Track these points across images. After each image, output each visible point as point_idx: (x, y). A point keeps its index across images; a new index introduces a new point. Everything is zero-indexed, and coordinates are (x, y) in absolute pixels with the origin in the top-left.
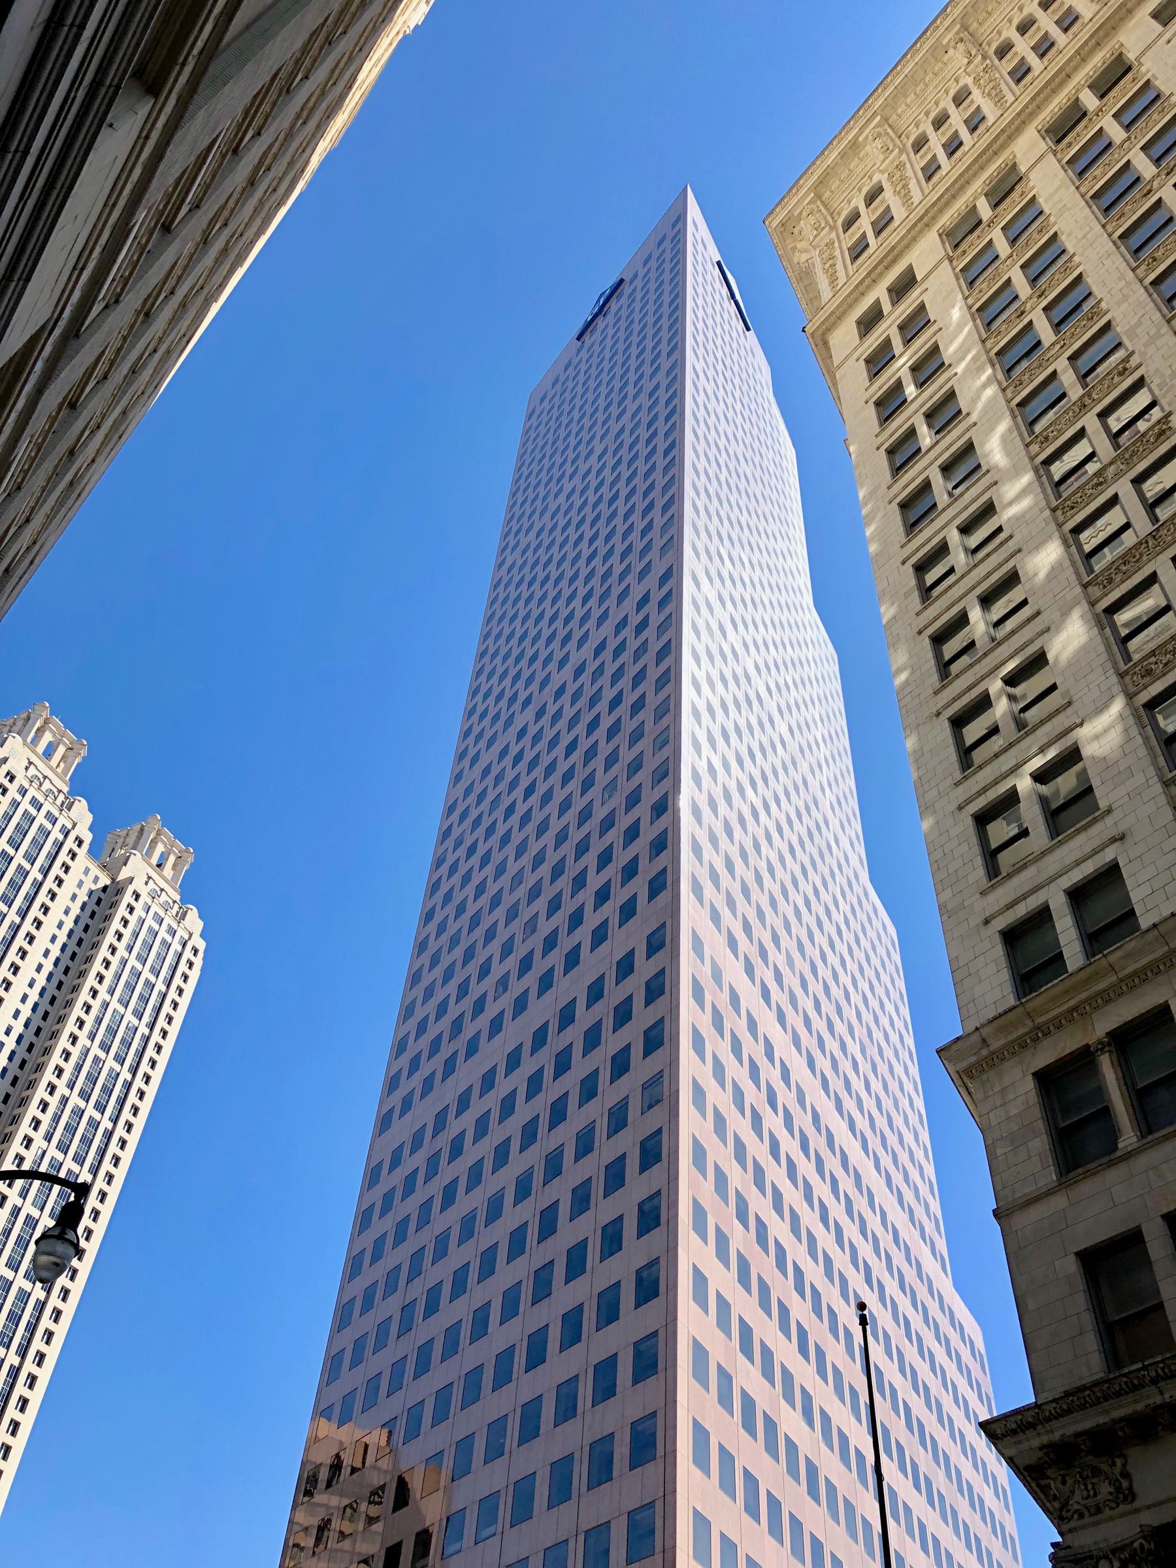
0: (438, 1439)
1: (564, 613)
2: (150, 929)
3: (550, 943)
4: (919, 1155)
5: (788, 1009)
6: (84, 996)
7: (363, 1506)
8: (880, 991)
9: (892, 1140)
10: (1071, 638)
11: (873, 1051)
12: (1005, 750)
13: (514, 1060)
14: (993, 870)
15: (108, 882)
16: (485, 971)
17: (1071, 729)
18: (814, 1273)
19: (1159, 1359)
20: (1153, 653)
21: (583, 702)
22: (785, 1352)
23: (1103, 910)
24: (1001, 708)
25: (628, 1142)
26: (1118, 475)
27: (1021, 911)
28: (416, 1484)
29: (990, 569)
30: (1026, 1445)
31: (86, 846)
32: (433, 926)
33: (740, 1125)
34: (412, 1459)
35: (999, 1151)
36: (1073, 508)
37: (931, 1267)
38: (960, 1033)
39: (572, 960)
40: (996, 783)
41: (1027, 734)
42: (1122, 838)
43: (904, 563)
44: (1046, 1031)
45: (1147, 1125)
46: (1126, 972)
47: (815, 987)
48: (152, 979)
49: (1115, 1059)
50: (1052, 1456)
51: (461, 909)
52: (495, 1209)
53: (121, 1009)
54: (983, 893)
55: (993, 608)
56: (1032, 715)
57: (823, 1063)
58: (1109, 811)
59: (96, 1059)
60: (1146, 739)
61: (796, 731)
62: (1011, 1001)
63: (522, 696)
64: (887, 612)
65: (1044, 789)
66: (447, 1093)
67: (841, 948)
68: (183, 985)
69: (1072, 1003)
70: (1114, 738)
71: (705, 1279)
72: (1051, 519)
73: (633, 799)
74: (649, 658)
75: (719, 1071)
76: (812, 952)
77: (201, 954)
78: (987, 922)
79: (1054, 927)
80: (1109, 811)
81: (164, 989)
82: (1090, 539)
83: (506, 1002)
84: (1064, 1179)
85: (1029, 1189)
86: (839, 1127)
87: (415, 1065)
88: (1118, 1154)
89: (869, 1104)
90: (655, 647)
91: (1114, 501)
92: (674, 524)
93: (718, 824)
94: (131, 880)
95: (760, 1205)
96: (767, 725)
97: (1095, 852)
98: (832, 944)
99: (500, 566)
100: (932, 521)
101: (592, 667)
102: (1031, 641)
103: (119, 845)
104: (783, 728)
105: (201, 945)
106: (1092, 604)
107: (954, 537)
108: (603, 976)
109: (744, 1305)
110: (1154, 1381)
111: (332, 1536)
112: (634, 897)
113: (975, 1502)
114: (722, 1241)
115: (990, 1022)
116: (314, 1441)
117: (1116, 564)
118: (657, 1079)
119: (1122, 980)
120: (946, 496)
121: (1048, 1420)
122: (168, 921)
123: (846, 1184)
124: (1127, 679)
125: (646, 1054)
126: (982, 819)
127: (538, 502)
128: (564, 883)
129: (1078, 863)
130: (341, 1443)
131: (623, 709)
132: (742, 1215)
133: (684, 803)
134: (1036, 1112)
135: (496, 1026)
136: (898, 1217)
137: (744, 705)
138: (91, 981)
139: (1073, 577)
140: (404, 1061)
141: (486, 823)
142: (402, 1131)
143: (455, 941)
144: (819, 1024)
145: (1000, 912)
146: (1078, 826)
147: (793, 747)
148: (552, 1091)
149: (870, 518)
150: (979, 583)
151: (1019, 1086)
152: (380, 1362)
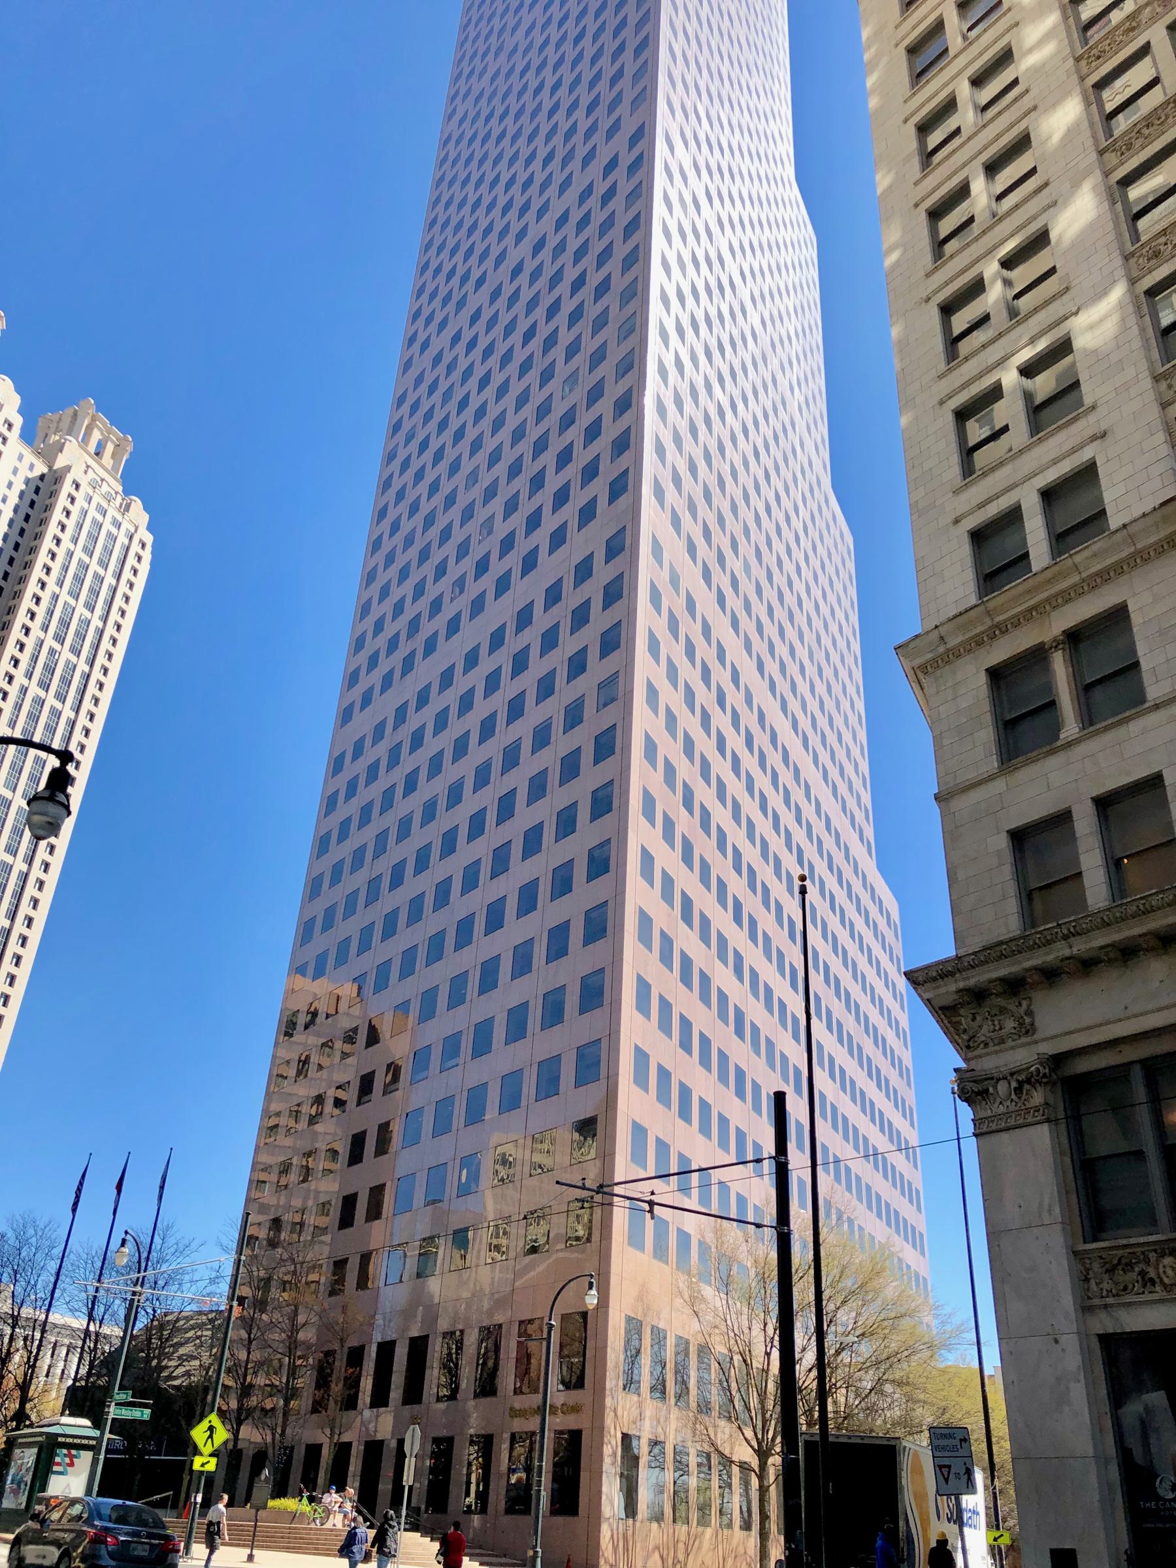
0: (409, 989)
1: (522, 178)
2: (94, 520)
3: (507, 544)
4: (856, 752)
5: (742, 615)
6: (32, 587)
7: (338, 1045)
8: (832, 598)
9: (832, 738)
10: (1079, 214)
11: (820, 656)
12: (992, 341)
13: (472, 659)
14: (968, 469)
15: (45, 470)
16: (441, 571)
17: (1065, 318)
18: (751, 854)
19: (1072, 918)
20: (1164, 232)
21: (542, 282)
22: (722, 920)
23: (1074, 510)
24: (995, 293)
25: (583, 737)
26: (1153, 19)
27: (993, 510)
28: (385, 1030)
29: (998, 133)
30: (943, 990)
31: (17, 430)
32: (386, 524)
33: (689, 722)
34: (381, 1008)
35: (946, 742)
36: (1099, 57)
37: (858, 850)
38: (919, 631)
39: (530, 563)
40: (980, 376)
41: (1018, 323)
42: (1104, 435)
43: (906, 121)
44: (1004, 629)
45: (1088, 718)
46: (1093, 570)
47: (770, 594)
48: (58, 705)
49: (1067, 657)
50: (966, 998)
51: (414, 508)
52: (455, 795)
53: (72, 602)
54: (956, 492)
55: (997, 177)
56: (1024, 303)
57: (772, 667)
58: (1093, 407)
59: (52, 651)
60: (1143, 330)
61: (768, 323)
62: (973, 600)
63: (476, 274)
64: (883, 180)
65: (1028, 383)
66: (406, 690)
67: (798, 555)
68: (116, 635)
69: (1032, 603)
70: (1110, 327)
71: (652, 858)
72: (1073, 69)
73: (595, 395)
74: (616, 233)
75: (672, 673)
76: (770, 559)
77: (149, 548)
78: (957, 521)
79: (1023, 526)
80: (1093, 407)
81: (114, 582)
82: (1113, 97)
83: (463, 603)
84: (1004, 767)
85: (971, 775)
86: (783, 726)
87: (373, 661)
88: (1059, 743)
89: (813, 705)
90: (622, 220)
91: (1145, 50)
92: (646, 71)
93: (683, 423)
94: (68, 469)
95: (705, 795)
96: (739, 315)
97: (1074, 451)
98: (789, 552)
99: (450, 118)
100: (942, 69)
101: (552, 242)
102: (1034, 218)
103: (53, 429)
104: (754, 319)
105: (149, 539)
106: (1107, 174)
107: (964, 89)
108: (560, 580)
109: (687, 881)
110: (1065, 937)
111: (312, 1068)
112: (595, 499)
113: (880, 1042)
114: (669, 826)
115: (950, 620)
116: (291, 992)
117: (1139, 126)
118: (613, 679)
119: (1083, 580)
120: (959, 39)
121: (965, 969)
122: (112, 512)
123: (785, 777)
124: (1132, 261)
125: (603, 655)
126: (962, 415)
127: (493, 39)
128: (522, 483)
129: (1055, 462)
130: (315, 994)
131: (586, 292)
132: (688, 802)
133: (649, 402)
134: (986, 706)
135: (453, 626)
136: (830, 806)
137: (716, 291)
138: (37, 572)
139: (1090, 142)
140: (363, 657)
141: (438, 416)
142: (363, 723)
143: (409, 541)
144: (771, 630)
145: (970, 513)
146: (1060, 423)
147: (764, 340)
148: (509, 688)
149: (873, 64)
150: (985, 148)
151: (971, 681)
152: (349, 928)
